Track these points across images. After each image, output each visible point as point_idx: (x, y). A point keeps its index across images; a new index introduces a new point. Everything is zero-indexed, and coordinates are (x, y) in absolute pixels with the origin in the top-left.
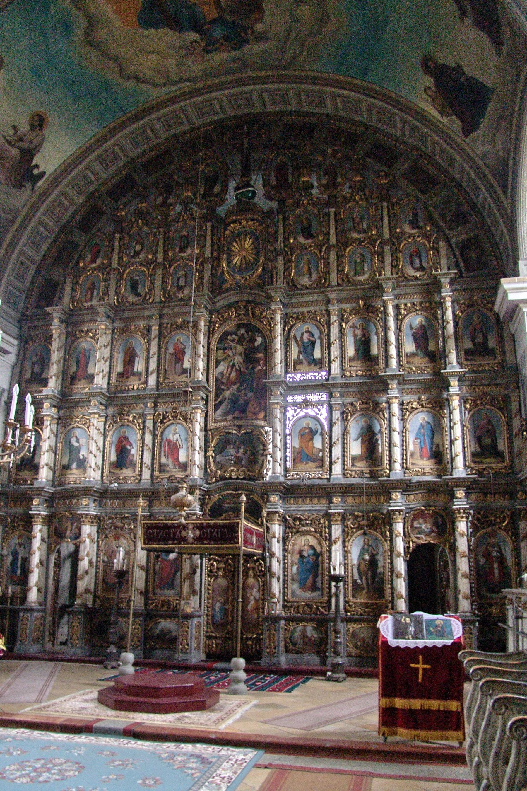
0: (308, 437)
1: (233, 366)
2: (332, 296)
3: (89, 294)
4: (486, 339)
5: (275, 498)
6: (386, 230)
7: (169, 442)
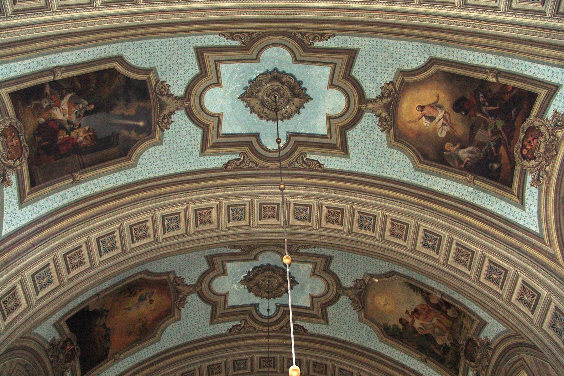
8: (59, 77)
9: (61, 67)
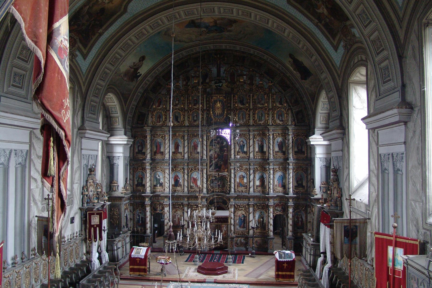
0: (242, 179)
1: (216, 152)
2: (251, 129)
3: (158, 120)
4: (302, 148)
5: (232, 200)
6: (270, 105)
7: (194, 178)
8: (316, 21)
9: (313, 23)
